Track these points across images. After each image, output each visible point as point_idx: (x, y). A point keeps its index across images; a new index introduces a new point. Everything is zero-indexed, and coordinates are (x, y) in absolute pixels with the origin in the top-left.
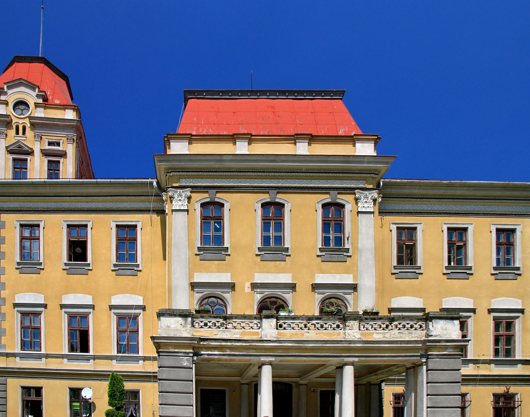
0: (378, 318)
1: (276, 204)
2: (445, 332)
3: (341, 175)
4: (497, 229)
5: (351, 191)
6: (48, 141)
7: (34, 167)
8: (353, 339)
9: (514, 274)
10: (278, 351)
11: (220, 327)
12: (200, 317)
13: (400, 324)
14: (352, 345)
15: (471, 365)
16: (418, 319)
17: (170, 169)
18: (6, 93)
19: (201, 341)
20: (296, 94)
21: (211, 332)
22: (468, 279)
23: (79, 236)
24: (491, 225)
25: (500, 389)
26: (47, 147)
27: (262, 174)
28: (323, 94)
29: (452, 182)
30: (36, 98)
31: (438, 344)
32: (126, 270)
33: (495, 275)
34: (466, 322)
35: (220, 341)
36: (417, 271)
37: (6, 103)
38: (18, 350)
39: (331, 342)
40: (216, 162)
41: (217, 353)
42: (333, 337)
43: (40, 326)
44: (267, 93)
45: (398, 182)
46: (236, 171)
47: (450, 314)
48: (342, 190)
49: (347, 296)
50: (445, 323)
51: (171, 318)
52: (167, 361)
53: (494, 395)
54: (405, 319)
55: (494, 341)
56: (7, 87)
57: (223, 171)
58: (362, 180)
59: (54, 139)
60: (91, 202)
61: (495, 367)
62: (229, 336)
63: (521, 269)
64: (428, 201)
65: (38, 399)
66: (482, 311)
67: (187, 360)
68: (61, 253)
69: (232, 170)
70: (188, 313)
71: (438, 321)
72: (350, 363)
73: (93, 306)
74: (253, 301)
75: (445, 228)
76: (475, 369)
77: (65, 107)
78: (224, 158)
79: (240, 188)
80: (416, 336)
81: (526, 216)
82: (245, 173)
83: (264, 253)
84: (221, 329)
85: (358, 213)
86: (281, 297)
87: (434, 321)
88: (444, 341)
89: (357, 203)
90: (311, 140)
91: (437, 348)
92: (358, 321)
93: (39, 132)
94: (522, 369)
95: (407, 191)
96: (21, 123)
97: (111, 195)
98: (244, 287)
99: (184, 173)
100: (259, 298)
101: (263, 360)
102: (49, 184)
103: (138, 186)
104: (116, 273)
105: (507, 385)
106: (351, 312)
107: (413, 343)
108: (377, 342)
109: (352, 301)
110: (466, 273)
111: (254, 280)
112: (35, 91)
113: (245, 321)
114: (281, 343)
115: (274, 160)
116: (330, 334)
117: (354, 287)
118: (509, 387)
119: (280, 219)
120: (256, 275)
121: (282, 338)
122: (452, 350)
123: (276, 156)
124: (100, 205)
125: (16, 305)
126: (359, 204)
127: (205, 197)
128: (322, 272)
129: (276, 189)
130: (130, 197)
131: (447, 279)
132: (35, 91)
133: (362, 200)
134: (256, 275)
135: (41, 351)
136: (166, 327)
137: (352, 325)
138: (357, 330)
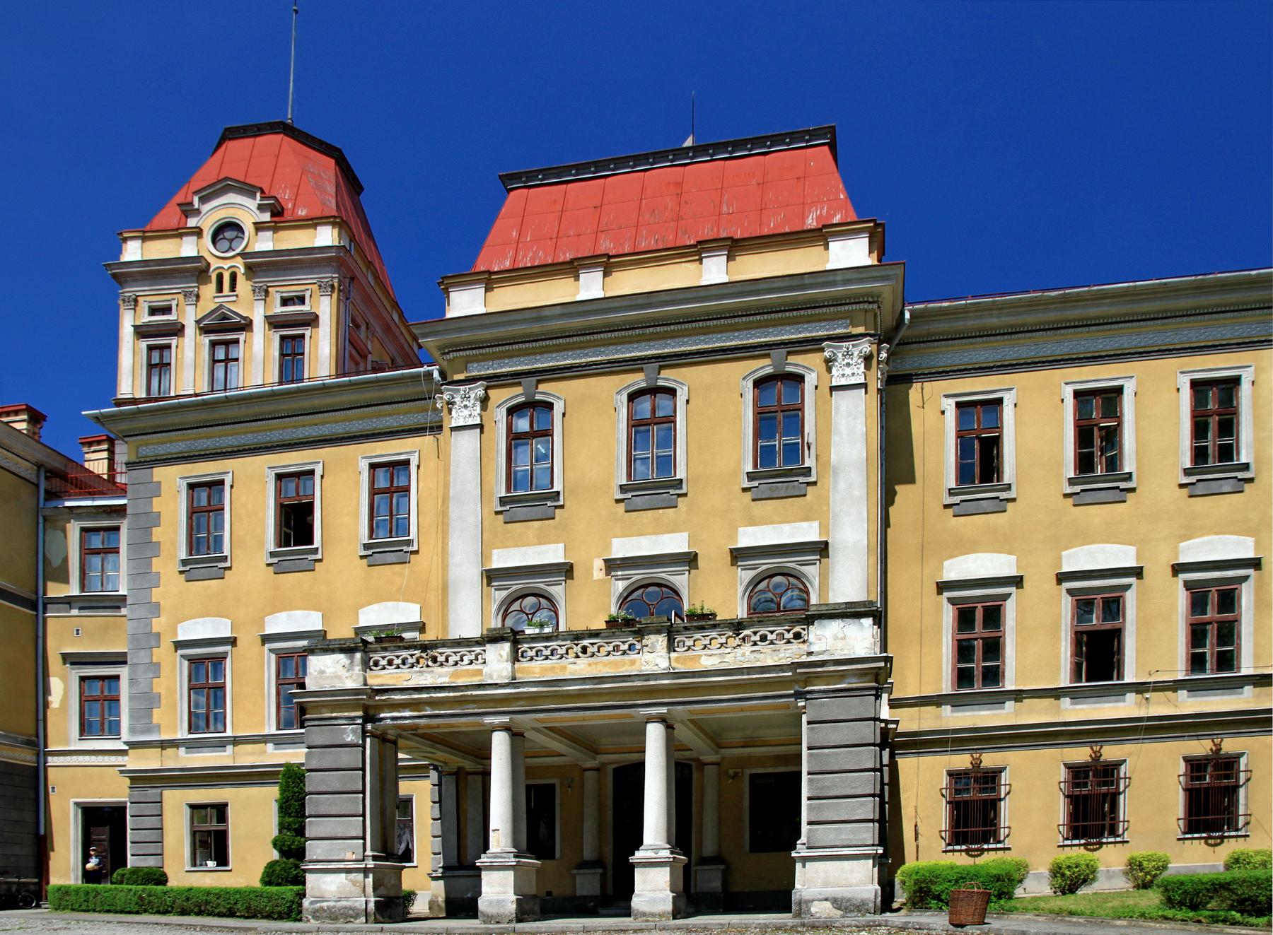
2: (840, 644)
5: (813, 345)
6: (281, 297)
9: (1235, 480)
12: (380, 649)
13: (755, 633)
14: (652, 683)
15: (1131, 697)
17: (446, 347)
18: (198, 212)
19: (376, 695)
20: (730, 149)
21: (398, 675)
22: (1124, 501)
23: (301, 494)
24: (1178, 374)
25: (1200, 747)
26: (279, 310)
28: (787, 140)
29: (1068, 293)
30: (257, 212)
31: (819, 670)
34: (1237, 591)
35: (409, 692)
36: (1003, 495)
37: (198, 232)
38: (182, 733)
39: (611, 679)
41: (407, 714)
42: (622, 670)
43: (224, 683)
44: (668, 156)
45: (945, 307)
49: (804, 569)
52: (319, 735)
53: (1187, 760)
55: (1190, 637)
56: (200, 198)
58: (842, 318)
60: (324, 424)
61: (1188, 697)
62: (431, 681)
63: (1252, 466)
64: (1030, 338)
65: (221, 827)
66: (1158, 572)
67: (353, 731)
68: (264, 533)
69: (567, 334)
71: (826, 622)
73: (323, 633)
74: (609, 596)
75: (1068, 392)
76: (1139, 705)
78: (546, 312)
81: (1265, 343)
82: (595, 336)
84: (415, 669)
85: (833, 389)
86: (669, 584)
89: (829, 370)
91: (823, 676)
93: (263, 280)
94: (1253, 697)
95: (972, 323)
96: (226, 267)
99: (474, 352)
100: (621, 589)
105: (1215, 737)
107: (775, 670)
109: (817, 579)
110: (1117, 488)
112: (255, 199)
113: (459, 650)
115: (646, 304)
116: (616, 664)
117: (821, 549)
120: (616, 542)
122: (855, 680)
125: (179, 645)
126: (834, 371)
127: (514, 394)
128: (752, 522)
131: (1074, 505)
132: (255, 199)
134: (616, 542)
135: (225, 731)
137: (652, 643)
138: (664, 652)
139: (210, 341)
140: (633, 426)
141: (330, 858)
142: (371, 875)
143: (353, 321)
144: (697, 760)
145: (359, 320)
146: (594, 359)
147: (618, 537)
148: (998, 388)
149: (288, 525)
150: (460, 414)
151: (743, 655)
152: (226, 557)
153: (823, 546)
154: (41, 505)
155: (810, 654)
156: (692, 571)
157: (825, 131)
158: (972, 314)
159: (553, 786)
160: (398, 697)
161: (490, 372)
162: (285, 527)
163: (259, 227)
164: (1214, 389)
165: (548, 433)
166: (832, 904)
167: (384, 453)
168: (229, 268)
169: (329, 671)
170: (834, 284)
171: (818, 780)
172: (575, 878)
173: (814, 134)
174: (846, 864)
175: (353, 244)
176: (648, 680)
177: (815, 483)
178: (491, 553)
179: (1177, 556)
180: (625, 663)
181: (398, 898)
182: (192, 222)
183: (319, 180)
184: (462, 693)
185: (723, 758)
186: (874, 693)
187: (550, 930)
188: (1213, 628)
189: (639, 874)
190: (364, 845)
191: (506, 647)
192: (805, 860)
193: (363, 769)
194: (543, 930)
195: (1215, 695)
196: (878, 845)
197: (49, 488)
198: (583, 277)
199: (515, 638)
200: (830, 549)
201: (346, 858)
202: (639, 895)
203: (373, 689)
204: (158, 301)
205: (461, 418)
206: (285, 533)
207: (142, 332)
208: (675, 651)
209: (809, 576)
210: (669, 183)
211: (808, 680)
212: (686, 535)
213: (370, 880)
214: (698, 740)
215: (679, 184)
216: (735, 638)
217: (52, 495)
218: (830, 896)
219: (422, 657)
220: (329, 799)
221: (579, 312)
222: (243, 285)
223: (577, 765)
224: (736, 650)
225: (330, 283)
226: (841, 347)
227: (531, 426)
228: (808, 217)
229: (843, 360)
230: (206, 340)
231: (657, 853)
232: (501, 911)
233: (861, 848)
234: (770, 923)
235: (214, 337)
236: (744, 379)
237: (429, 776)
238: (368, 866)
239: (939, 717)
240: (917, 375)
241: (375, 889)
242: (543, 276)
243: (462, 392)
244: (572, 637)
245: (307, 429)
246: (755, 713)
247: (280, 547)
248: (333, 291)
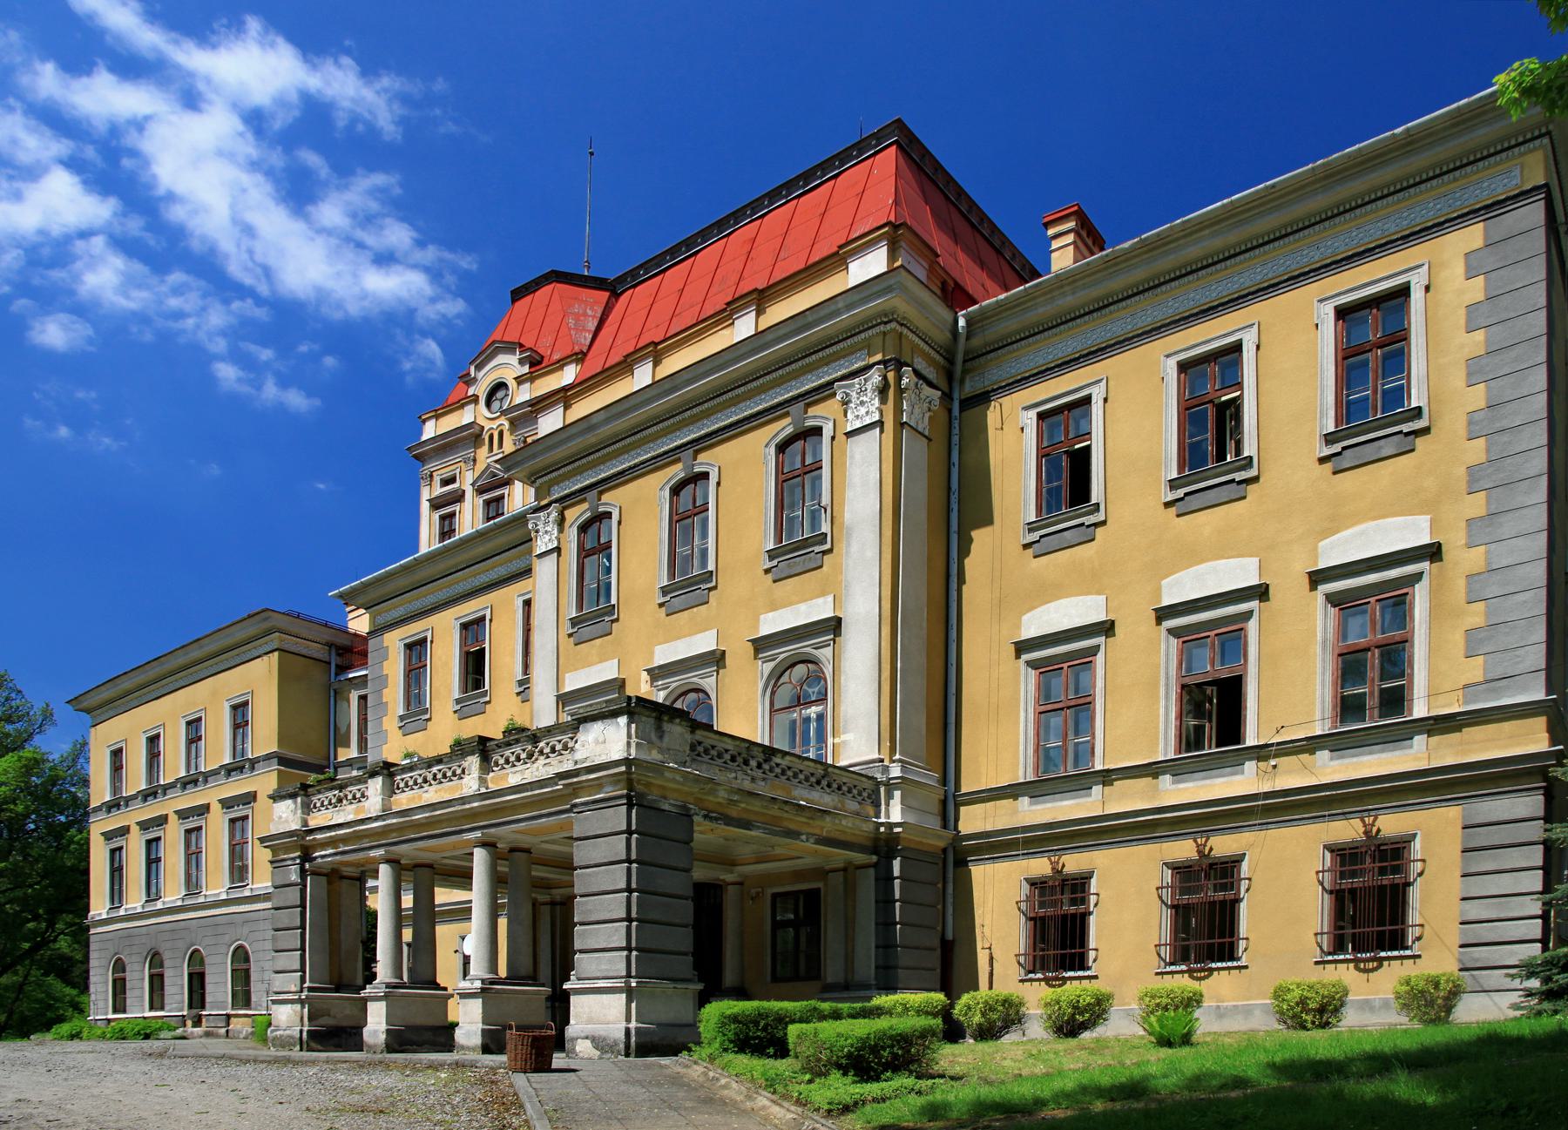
2: (599, 749)
4: (1340, 308)
5: (824, 391)
9: (1399, 436)
14: (467, 806)
18: (475, 379)
25: (1348, 830)
27: (672, 421)
29: (1145, 238)
31: (575, 780)
33: (1333, 459)
34: (1408, 597)
37: (475, 399)
56: (476, 367)
61: (1332, 759)
71: (588, 725)
78: (595, 420)
81: (1447, 225)
88: (583, 771)
105: (1366, 814)
110: (1233, 481)
112: (515, 354)
118: (1372, 818)
120: (658, 649)
122: (610, 789)
128: (773, 606)
131: (1178, 516)
132: (515, 354)
134: (658, 649)
140: (677, 522)
148: (1084, 384)
154: (332, 680)
158: (1042, 299)
163: (520, 380)
164: (1375, 311)
169: (284, 816)
170: (837, 313)
176: (464, 804)
179: (1315, 558)
182: (471, 392)
186: (625, 801)
188: (1373, 655)
195: (1371, 753)
197: (340, 663)
204: (446, 473)
207: (436, 504)
209: (823, 659)
211: (576, 790)
217: (343, 669)
226: (853, 385)
235: (487, 496)
236: (766, 446)
239: (1015, 812)
240: (994, 390)
241: (310, 1019)
242: (608, 381)
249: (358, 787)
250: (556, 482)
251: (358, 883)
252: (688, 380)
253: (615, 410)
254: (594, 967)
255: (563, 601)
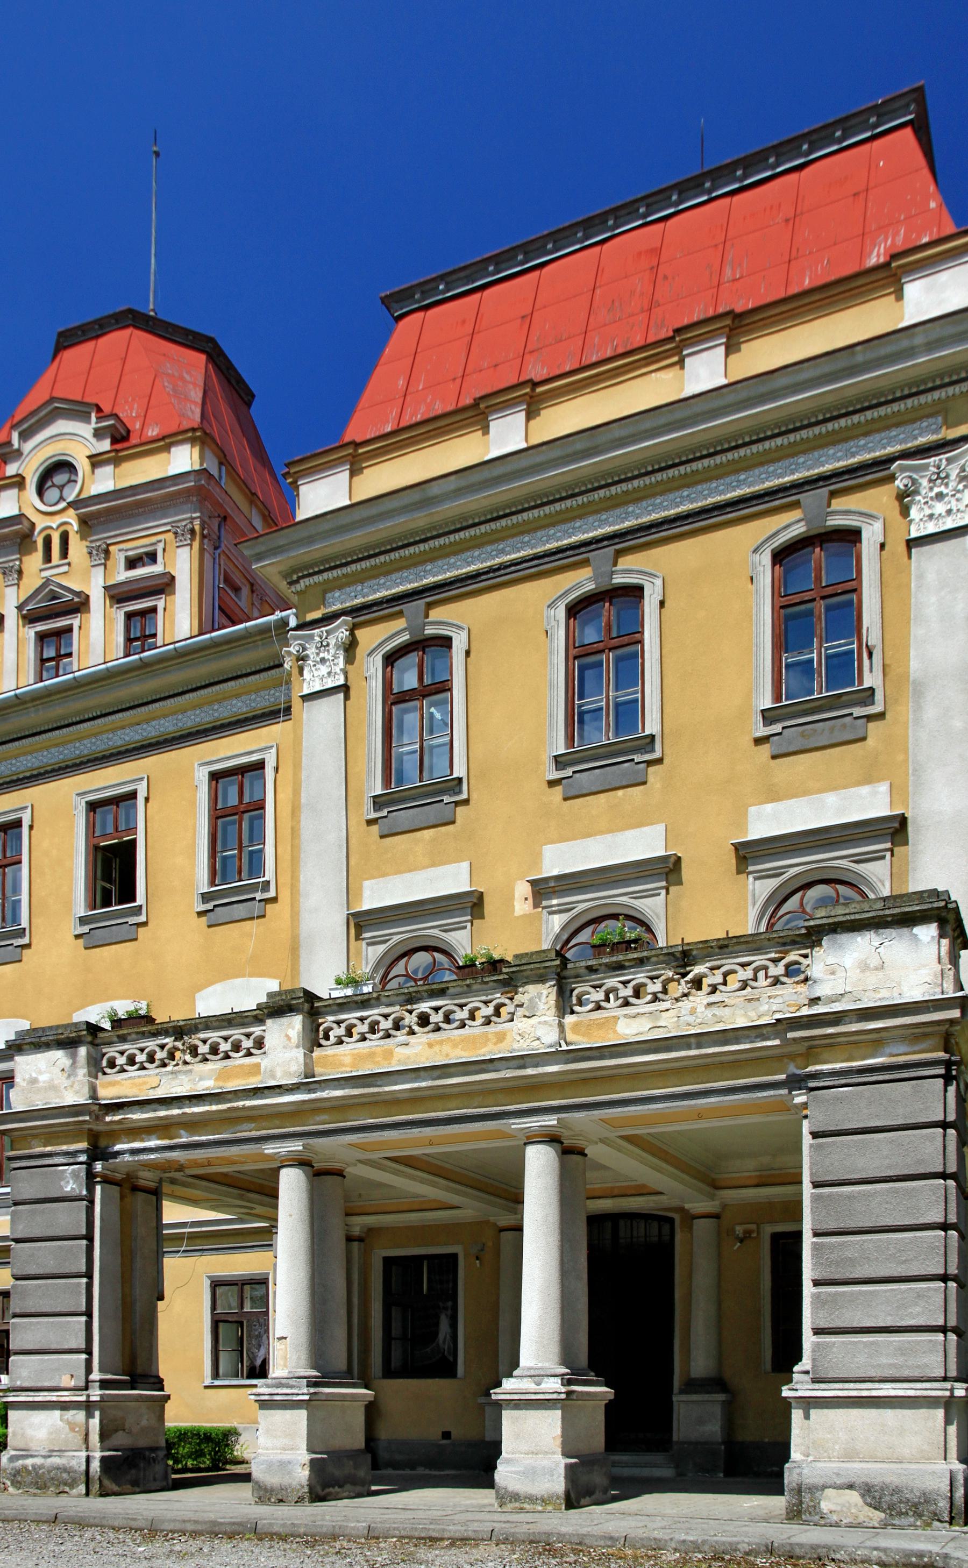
0: (630, 960)
1: (620, 592)
2: (872, 979)
3: (843, 422)
7: (88, 645)
8: (533, 1050)
10: (318, 1119)
11: (166, 1061)
12: (115, 1039)
14: (530, 1071)
16: (781, 940)
17: (294, 570)
18: (18, 453)
19: (107, 1114)
21: (141, 1080)
23: (122, 827)
30: (93, 440)
31: (830, 1030)
32: (235, 906)
37: (19, 482)
39: (461, 1068)
40: (413, 510)
41: (152, 1143)
42: (483, 1051)
46: (483, 519)
47: (898, 904)
48: (846, 477)
49: (865, 869)
50: (877, 944)
51: (39, 1055)
54: (730, 949)
56: (20, 434)
57: (447, 530)
59: (138, 547)
60: (147, 721)
62: (188, 1088)
69: (470, 522)
70: (74, 1035)
71: (844, 938)
72: (535, 1136)
77: (167, 441)
78: (435, 490)
79: (497, 574)
80: (774, 1009)
83: (574, 772)
84: (169, 1068)
85: (911, 544)
87: (829, 940)
90: (735, 332)
91: (839, 1044)
92: (552, 983)
96: (54, 526)
97: (194, 686)
98: (512, 898)
100: (557, 929)
101: (271, 1151)
102: (34, 699)
103: (254, 642)
104: (208, 921)
106: (527, 954)
108: (613, 1049)
111: (540, 870)
112: (89, 422)
114: (314, 1091)
116: (472, 1042)
119: (633, 641)
120: (549, 851)
121: (325, 1075)
122: (902, 1049)
123: (593, 431)
124: (168, 726)
126: (914, 513)
128: (773, 795)
129: (611, 542)
130: (245, 679)
132: (89, 422)
133: (923, 492)
134: (549, 851)
136: (28, 1084)
137: (531, 1000)
139: (36, 633)
140: (575, 658)
141: (39, 1384)
142: (97, 1414)
143: (227, 580)
144: (681, 1210)
145: (238, 579)
146: (513, 556)
147: (552, 842)
149: (107, 877)
150: (316, 674)
151: (693, 1012)
152: (24, 929)
153: (896, 825)
155: (815, 1001)
156: (672, 889)
157: (902, 102)
159: (454, 1257)
160: (137, 1116)
161: (359, 601)
162: (103, 879)
163: (96, 461)
165: (444, 687)
166: (863, 1496)
167: (229, 754)
168: (58, 527)
169: (43, 1078)
170: (910, 353)
171: (832, 1247)
172: (484, 1410)
173: (882, 112)
174: (889, 1415)
175: (224, 468)
177: (881, 716)
178: (360, 888)
180: (488, 1040)
181: (154, 1449)
183: (180, 383)
184: (229, 1105)
185: (724, 1206)
186: (942, 1071)
187: (314, 1530)
189: (508, 1418)
190: (89, 1363)
191: (295, 1024)
192: (809, 1404)
193: (89, 1238)
194: (302, 1530)
196: (957, 1380)
198: (496, 426)
199: (312, 1007)
200: (910, 829)
201: (63, 1385)
202: (508, 1461)
203: (100, 1104)
205: (317, 679)
206: (104, 889)
208: (572, 1012)
210: (640, 254)
211: (812, 1051)
212: (661, 828)
213: (95, 1422)
214: (658, 1175)
215: (657, 252)
216: (678, 981)
218: (858, 1481)
219: (177, 1049)
220: (39, 1286)
221: (486, 481)
222: (77, 547)
223: (488, 1222)
224: (680, 1004)
225: (189, 526)
226: (926, 467)
227: (421, 678)
228: (871, 252)
229: (931, 489)
230: (30, 633)
231: (538, 1384)
232: (286, 1481)
233: (919, 1385)
234: (704, 1542)
235: (41, 627)
237: (9, 1263)
238: (93, 1399)
241: (103, 1436)
243: (317, 639)
244: (403, 998)
245: (127, 731)
246: (727, 1122)
247: (95, 909)
248: (192, 539)
249: (225, 1033)
250: (339, 584)
251: (154, 1198)
252: (620, 439)
253: (475, 477)
254: (861, 1359)
255: (358, 767)
